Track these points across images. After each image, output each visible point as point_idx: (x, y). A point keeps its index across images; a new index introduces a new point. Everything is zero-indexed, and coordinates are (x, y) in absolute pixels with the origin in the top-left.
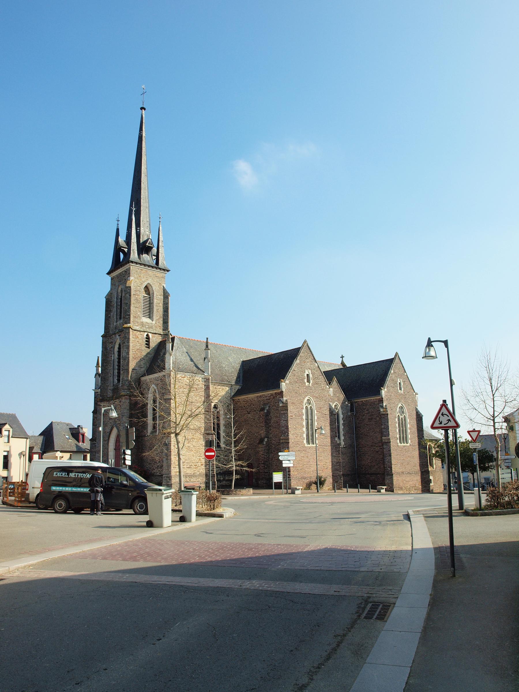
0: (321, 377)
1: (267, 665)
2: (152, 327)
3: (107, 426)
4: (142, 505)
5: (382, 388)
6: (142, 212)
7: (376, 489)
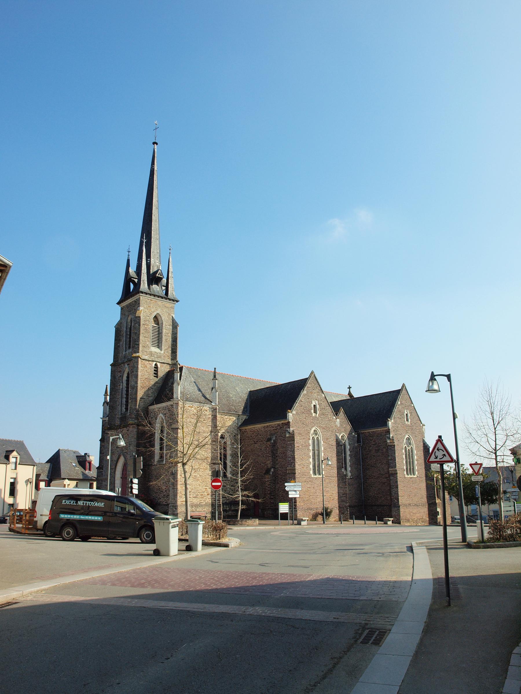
0: (327, 408)
1: (267, 683)
2: (160, 357)
3: (114, 454)
4: (149, 533)
5: (388, 419)
6: (152, 243)
7: (382, 521)
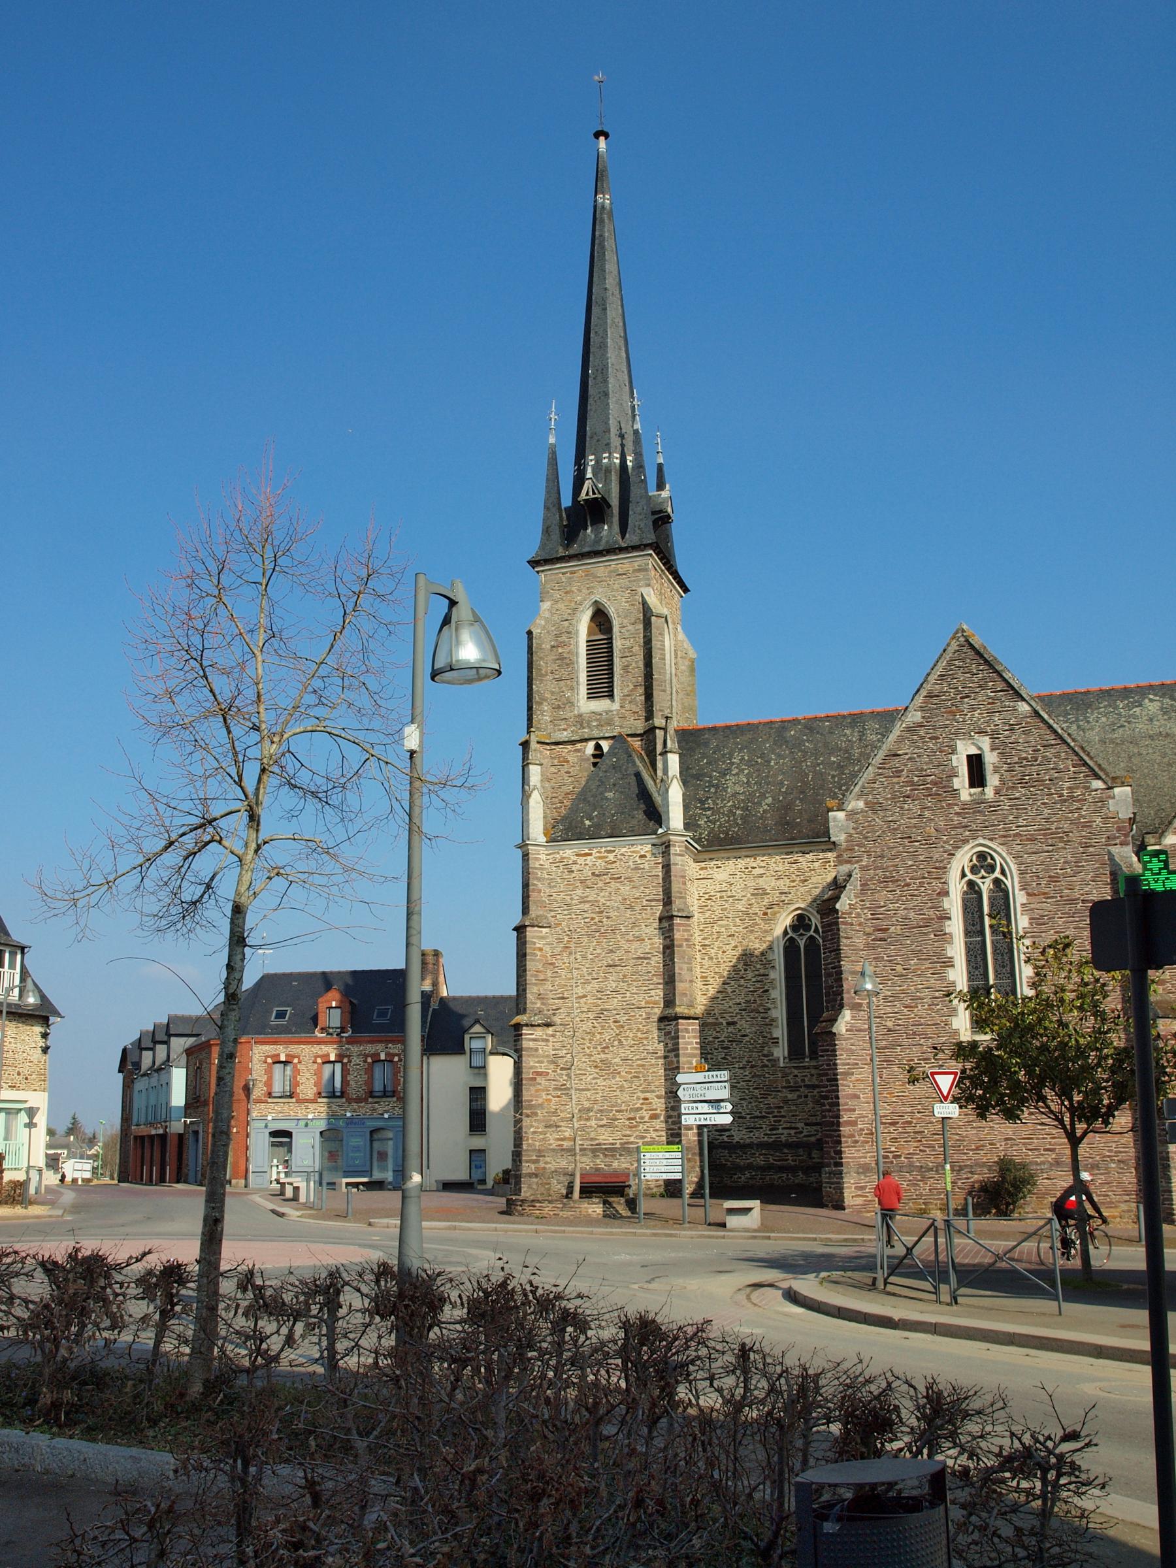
2: (609, 722)
